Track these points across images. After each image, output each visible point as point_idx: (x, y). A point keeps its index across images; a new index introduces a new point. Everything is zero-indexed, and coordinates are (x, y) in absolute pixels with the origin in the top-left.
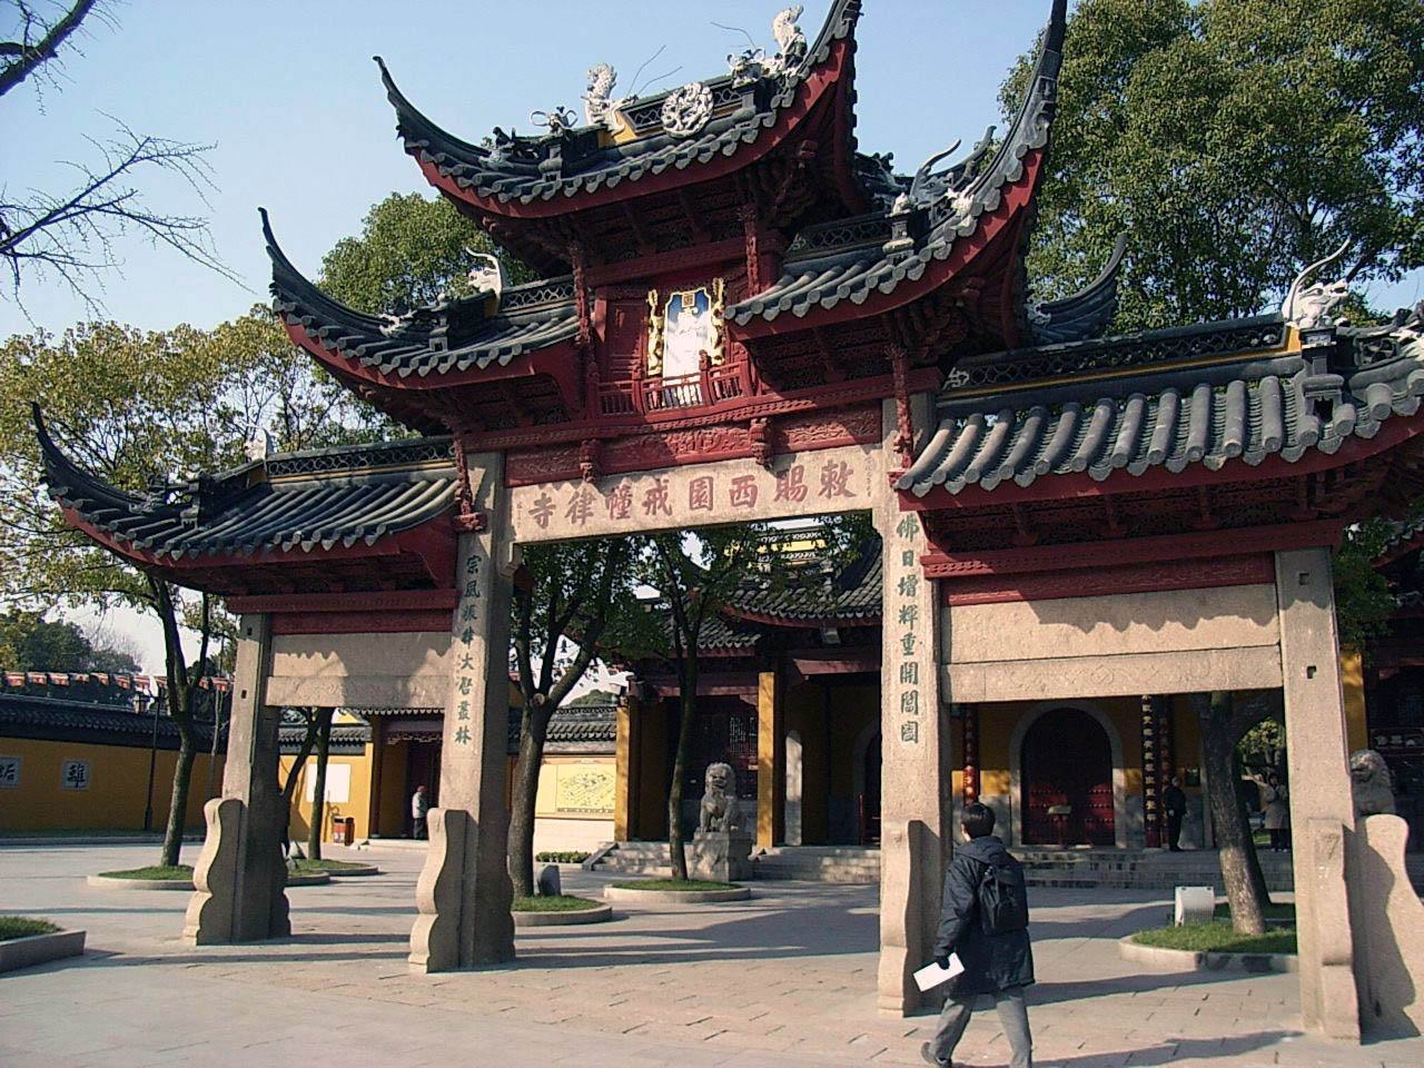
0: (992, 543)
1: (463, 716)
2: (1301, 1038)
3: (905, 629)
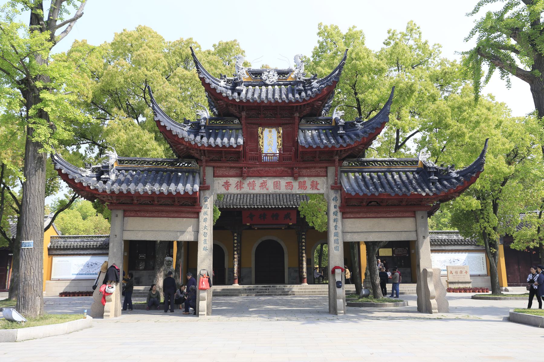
0: (354, 206)
2: (541, 229)
3: (335, 224)
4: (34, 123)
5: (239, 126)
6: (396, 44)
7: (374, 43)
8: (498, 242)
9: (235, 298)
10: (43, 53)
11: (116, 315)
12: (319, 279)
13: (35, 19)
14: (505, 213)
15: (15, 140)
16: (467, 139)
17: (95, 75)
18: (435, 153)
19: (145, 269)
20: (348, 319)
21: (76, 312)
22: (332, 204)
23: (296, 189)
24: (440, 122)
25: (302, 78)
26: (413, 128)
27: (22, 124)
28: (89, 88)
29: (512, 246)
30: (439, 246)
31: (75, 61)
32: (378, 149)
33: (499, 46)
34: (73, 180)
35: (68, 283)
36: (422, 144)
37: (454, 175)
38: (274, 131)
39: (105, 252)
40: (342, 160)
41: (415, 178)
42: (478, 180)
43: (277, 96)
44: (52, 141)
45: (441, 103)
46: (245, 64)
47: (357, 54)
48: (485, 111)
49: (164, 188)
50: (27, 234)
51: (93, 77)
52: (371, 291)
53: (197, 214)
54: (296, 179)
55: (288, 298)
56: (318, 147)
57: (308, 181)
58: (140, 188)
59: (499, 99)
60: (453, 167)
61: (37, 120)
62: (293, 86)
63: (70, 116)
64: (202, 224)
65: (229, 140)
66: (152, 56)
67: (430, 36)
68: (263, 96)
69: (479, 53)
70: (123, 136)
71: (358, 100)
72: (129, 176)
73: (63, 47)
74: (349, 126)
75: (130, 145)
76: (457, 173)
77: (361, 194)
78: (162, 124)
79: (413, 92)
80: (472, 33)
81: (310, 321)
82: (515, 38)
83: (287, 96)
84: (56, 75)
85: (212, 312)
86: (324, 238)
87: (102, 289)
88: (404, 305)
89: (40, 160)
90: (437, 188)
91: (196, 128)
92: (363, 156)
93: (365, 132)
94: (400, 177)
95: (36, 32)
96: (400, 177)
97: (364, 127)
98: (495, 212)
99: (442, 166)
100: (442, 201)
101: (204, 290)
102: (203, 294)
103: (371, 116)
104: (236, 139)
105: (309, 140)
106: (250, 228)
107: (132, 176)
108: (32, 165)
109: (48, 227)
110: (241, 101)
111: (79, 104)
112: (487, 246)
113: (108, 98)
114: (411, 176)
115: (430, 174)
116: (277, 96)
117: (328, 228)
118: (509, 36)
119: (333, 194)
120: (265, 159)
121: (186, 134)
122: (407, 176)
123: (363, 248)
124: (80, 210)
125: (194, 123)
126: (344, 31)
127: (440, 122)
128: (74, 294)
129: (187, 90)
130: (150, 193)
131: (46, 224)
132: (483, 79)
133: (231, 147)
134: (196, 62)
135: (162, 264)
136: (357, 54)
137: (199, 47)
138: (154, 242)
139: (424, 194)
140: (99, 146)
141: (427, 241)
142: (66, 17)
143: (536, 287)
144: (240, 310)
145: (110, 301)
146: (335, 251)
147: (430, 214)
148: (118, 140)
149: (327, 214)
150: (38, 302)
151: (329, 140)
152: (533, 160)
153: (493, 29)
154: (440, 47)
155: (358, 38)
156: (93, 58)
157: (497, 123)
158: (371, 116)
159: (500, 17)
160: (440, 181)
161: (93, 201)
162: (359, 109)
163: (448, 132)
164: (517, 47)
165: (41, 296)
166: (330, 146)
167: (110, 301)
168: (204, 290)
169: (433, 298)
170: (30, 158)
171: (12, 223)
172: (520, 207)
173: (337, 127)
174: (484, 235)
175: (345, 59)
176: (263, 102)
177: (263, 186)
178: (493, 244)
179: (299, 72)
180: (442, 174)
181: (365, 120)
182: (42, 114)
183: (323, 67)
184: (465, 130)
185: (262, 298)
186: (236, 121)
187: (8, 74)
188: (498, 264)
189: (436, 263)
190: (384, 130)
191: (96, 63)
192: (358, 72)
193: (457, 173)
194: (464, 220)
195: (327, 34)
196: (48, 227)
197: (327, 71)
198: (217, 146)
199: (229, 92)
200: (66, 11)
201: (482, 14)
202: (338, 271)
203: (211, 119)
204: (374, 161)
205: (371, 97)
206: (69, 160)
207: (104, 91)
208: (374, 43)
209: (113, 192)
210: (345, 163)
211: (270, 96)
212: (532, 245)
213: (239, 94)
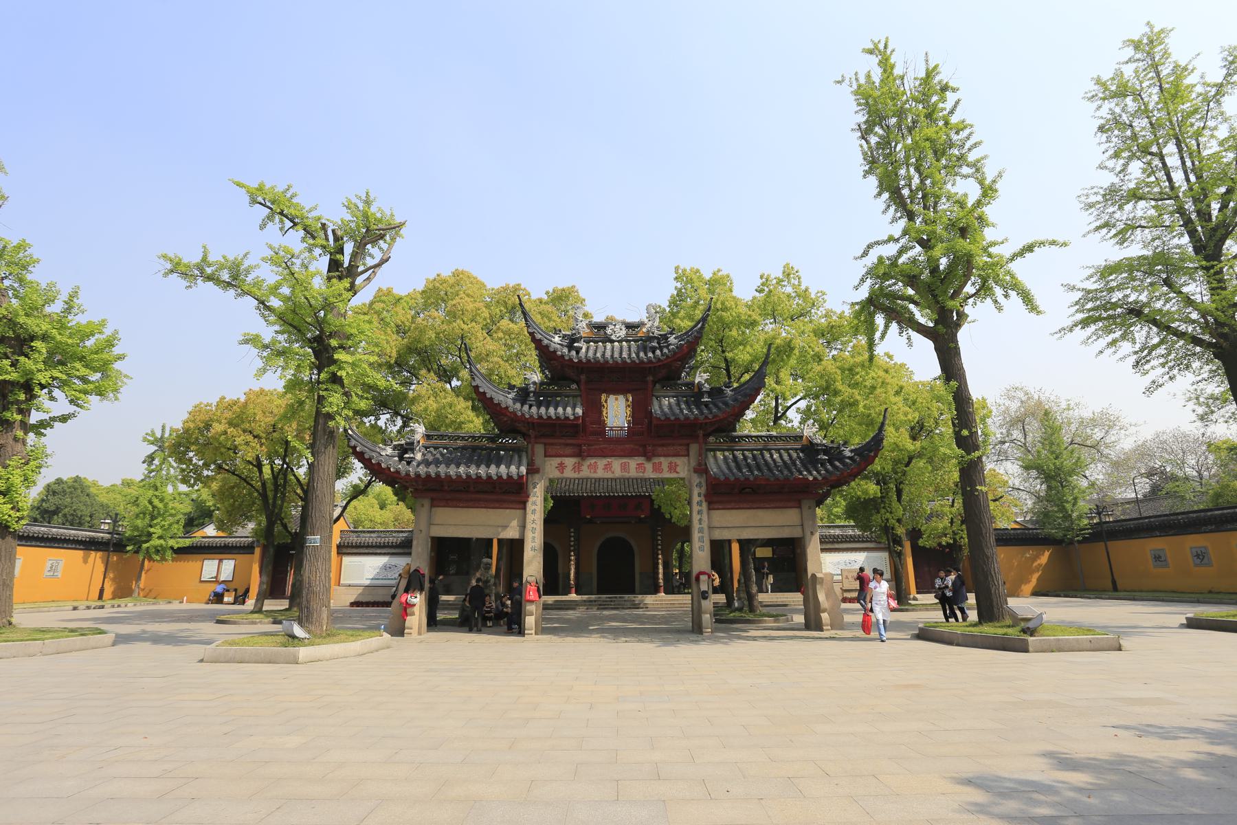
0: (723, 493)
4: (326, 390)
5: (578, 393)
6: (770, 291)
7: (745, 291)
8: (904, 538)
9: (571, 612)
10: (340, 304)
11: (420, 633)
12: (679, 587)
13: (334, 265)
14: (911, 500)
15: (303, 410)
16: (861, 409)
17: (400, 330)
18: (823, 426)
19: (457, 574)
20: (716, 640)
21: (371, 628)
22: (696, 491)
23: (650, 473)
24: (828, 388)
25: (657, 333)
26: (795, 395)
27: (311, 391)
28: (393, 345)
29: (921, 542)
30: (831, 544)
31: (378, 313)
32: (752, 421)
33: (894, 296)
34: (370, 460)
35: (360, 590)
36: (807, 414)
37: (848, 454)
38: (621, 398)
39: (406, 551)
40: (707, 435)
41: (799, 457)
42: (877, 460)
43: (625, 355)
44: (346, 411)
45: (828, 364)
46: (585, 315)
47: (723, 303)
48: (881, 373)
49: (482, 471)
50: (313, 528)
51: (398, 333)
52: (746, 603)
53: (522, 505)
54: (649, 459)
55: (640, 612)
56: (677, 419)
57: (665, 462)
58: (452, 471)
59: (898, 359)
60: (846, 443)
61: (329, 386)
62: (646, 342)
63: (369, 381)
64: (530, 517)
65: (564, 410)
66: (470, 307)
67: (811, 282)
68: (608, 354)
69: (872, 304)
70: (432, 404)
71: (726, 360)
72: (438, 456)
73: (364, 297)
74: (716, 392)
75: (440, 416)
76: (851, 451)
77: (732, 478)
78: (481, 390)
79: (792, 349)
80: (863, 280)
81: (666, 643)
82: (912, 287)
83: (638, 355)
84: (354, 331)
85: (541, 630)
86: (685, 533)
87: (403, 599)
88: (787, 620)
89: (331, 434)
90: (826, 470)
91: (523, 394)
92: (735, 430)
93: (735, 400)
94: (781, 456)
95: (334, 281)
96: (781, 456)
98: (899, 500)
99: (832, 442)
100: (833, 487)
101: (532, 601)
102: (531, 608)
103: (743, 380)
104: (574, 408)
105: (666, 410)
106: (590, 521)
107: (442, 455)
108: (322, 441)
109: (338, 519)
110: (580, 361)
111: (380, 365)
112: (888, 540)
113: (416, 358)
114: (795, 455)
115: (818, 452)
116: (625, 355)
117: (690, 521)
118: (906, 285)
119: (696, 479)
120: (609, 434)
121: (510, 402)
122: (789, 455)
123: (735, 548)
124: (378, 497)
125: (520, 389)
126: (707, 275)
127: (828, 388)
128: (367, 604)
129: (513, 347)
130: (464, 476)
131: (336, 514)
132: (878, 335)
133: (567, 418)
134: (525, 313)
135: (478, 568)
136: (723, 303)
137: (529, 294)
138: (468, 540)
139: (811, 478)
140: (402, 417)
141: (817, 536)
142: (370, 262)
143: (949, 594)
144: (578, 628)
145: (413, 614)
147: (819, 503)
148: (426, 410)
149: (690, 503)
150: (325, 615)
151: (690, 410)
152: (941, 434)
153: (886, 276)
154: (824, 294)
155: (725, 284)
156: (399, 309)
157: (896, 388)
158: (743, 380)
159: (894, 261)
160: (830, 461)
161: (393, 486)
162: (728, 370)
163: (838, 399)
164: (916, 298)
165: (328, 606)
166: (692, 417)
167: (413, 614)
168: (532, 601)
169: (824, 611)
170: (320, 433)
171: (295, 512)
172: (928, 492)
173: (700, 393)
174: (887, 529)
175: (709, 310)
176: (607, 362)
178: (897, 541)
179: (654, 326)
180: (833, 453)
181: (735, 385)
182: (336, 379)
183: (682, 320)
184: (859, 398)
185: (606, 613)
186: (574, 386)
187: (299, 331)
188: (904, 565)
189: (832, 566)
190: (759, 398)
191: (402, 315)
192: (726, 326)
193: (851, 451)
194: (860, 510)
195: (686, 279)
196: (338, 519)
197: (687, 324)
198: (550, 418)
199: (566, 350)
200: (370, 255)
201: (872, 258)
202: (703, 578)
203: (542, 383)
204: (747, 437)
205: (742, 355)
206: (365, 435)
207: (410, 350)
208: (745, 291)
209: (418, 475)
210: (711, 439)
211: (616, 355)
212: (944, 541)
213: (578, 353)
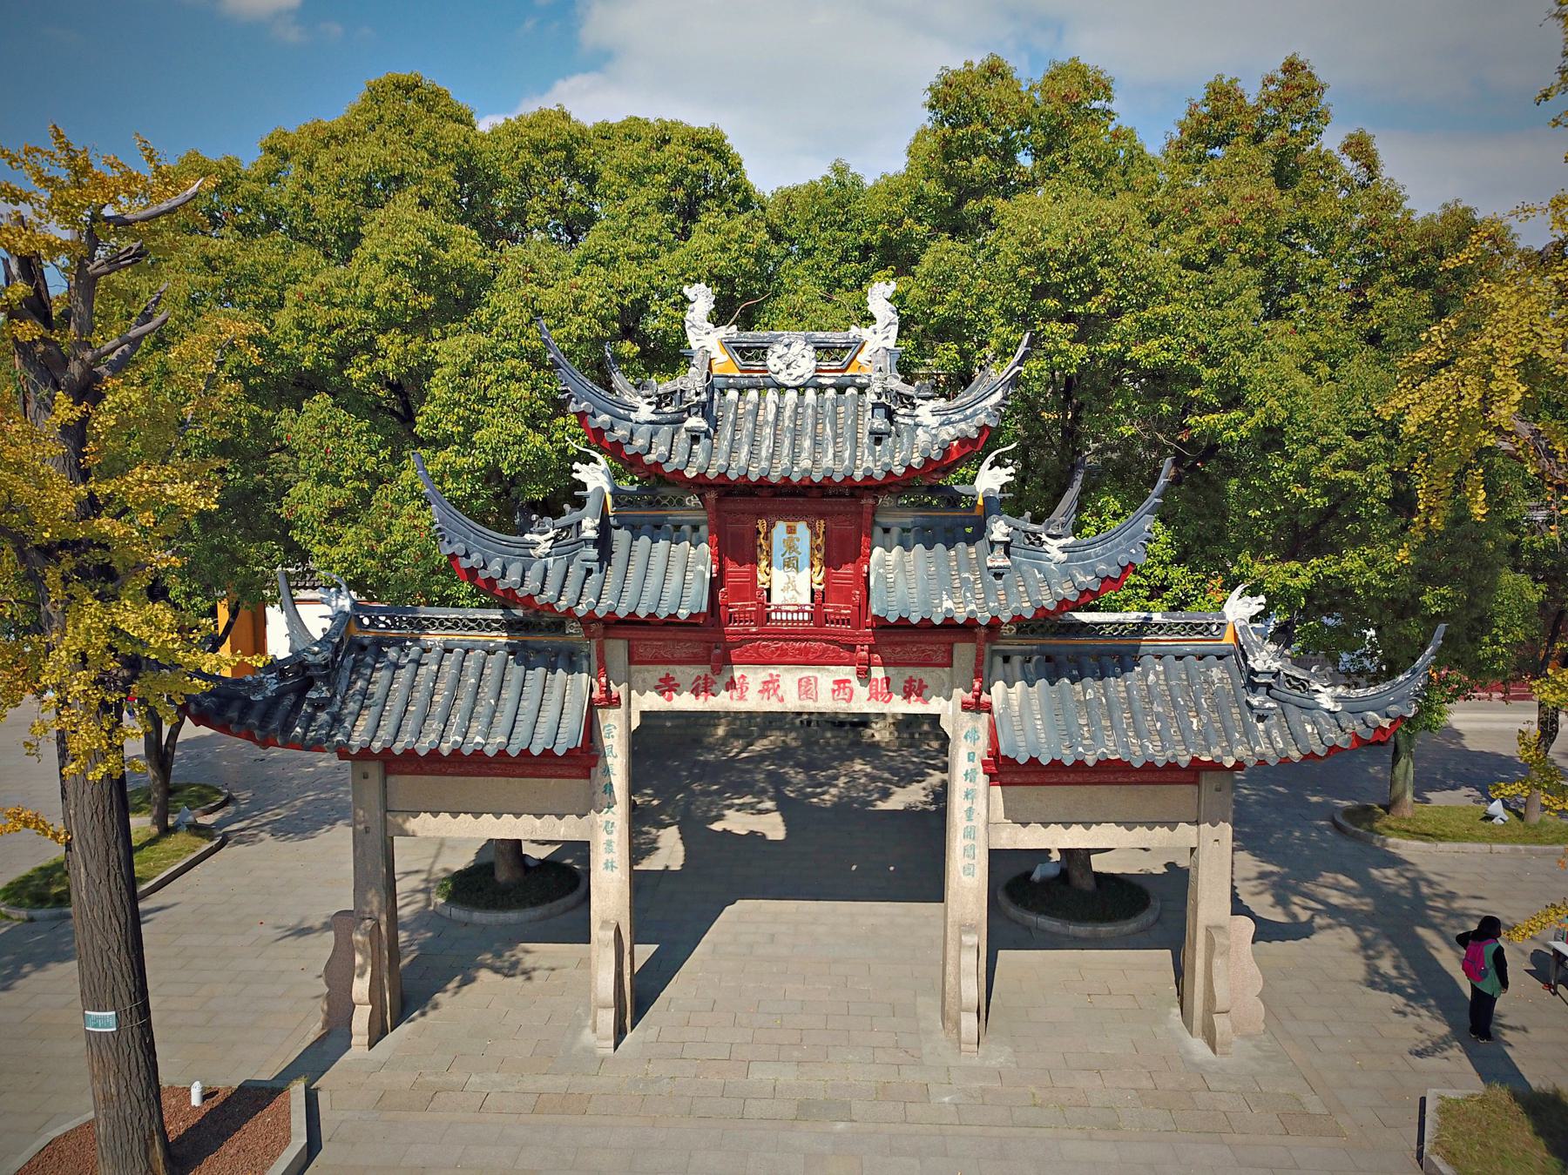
1: (609, 843)
3: (967, 804)
97: (1069, 560)
146: (965, 878)
177: (768, 690)
